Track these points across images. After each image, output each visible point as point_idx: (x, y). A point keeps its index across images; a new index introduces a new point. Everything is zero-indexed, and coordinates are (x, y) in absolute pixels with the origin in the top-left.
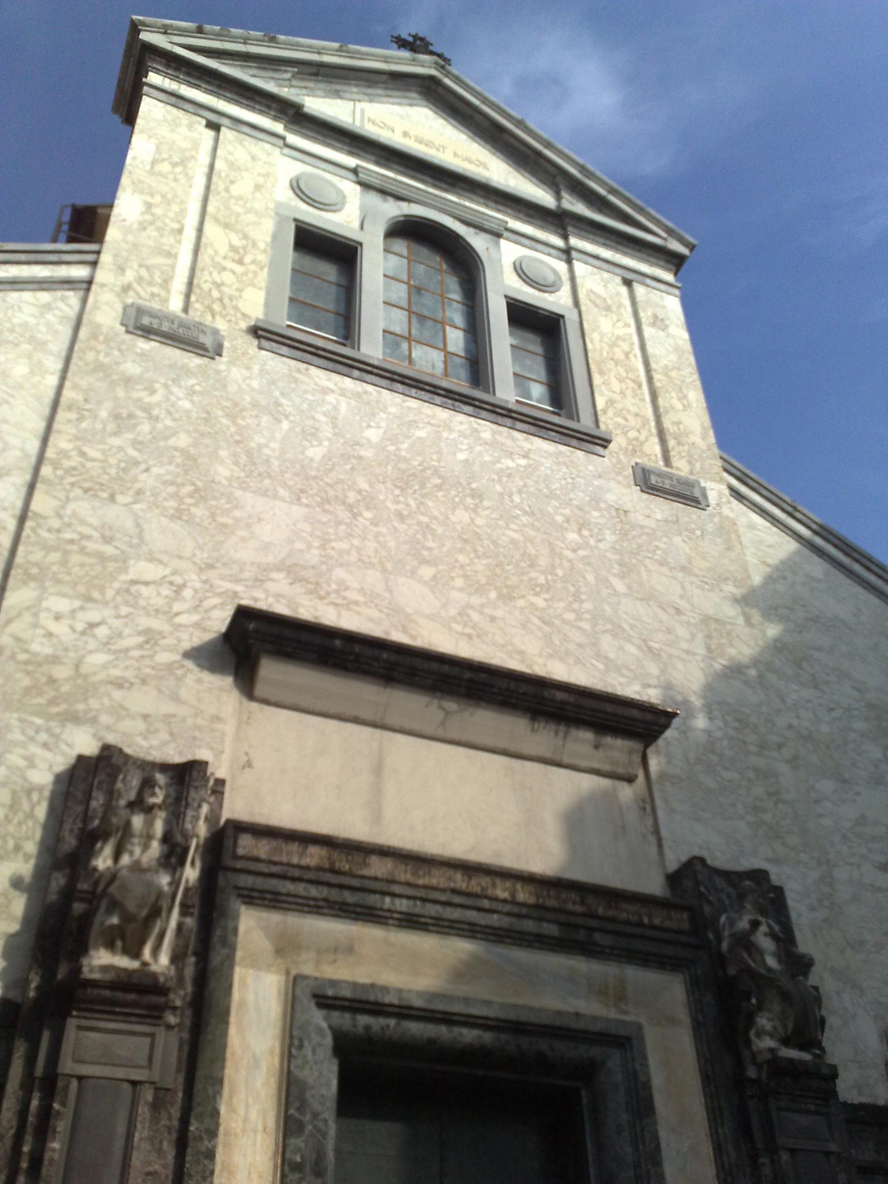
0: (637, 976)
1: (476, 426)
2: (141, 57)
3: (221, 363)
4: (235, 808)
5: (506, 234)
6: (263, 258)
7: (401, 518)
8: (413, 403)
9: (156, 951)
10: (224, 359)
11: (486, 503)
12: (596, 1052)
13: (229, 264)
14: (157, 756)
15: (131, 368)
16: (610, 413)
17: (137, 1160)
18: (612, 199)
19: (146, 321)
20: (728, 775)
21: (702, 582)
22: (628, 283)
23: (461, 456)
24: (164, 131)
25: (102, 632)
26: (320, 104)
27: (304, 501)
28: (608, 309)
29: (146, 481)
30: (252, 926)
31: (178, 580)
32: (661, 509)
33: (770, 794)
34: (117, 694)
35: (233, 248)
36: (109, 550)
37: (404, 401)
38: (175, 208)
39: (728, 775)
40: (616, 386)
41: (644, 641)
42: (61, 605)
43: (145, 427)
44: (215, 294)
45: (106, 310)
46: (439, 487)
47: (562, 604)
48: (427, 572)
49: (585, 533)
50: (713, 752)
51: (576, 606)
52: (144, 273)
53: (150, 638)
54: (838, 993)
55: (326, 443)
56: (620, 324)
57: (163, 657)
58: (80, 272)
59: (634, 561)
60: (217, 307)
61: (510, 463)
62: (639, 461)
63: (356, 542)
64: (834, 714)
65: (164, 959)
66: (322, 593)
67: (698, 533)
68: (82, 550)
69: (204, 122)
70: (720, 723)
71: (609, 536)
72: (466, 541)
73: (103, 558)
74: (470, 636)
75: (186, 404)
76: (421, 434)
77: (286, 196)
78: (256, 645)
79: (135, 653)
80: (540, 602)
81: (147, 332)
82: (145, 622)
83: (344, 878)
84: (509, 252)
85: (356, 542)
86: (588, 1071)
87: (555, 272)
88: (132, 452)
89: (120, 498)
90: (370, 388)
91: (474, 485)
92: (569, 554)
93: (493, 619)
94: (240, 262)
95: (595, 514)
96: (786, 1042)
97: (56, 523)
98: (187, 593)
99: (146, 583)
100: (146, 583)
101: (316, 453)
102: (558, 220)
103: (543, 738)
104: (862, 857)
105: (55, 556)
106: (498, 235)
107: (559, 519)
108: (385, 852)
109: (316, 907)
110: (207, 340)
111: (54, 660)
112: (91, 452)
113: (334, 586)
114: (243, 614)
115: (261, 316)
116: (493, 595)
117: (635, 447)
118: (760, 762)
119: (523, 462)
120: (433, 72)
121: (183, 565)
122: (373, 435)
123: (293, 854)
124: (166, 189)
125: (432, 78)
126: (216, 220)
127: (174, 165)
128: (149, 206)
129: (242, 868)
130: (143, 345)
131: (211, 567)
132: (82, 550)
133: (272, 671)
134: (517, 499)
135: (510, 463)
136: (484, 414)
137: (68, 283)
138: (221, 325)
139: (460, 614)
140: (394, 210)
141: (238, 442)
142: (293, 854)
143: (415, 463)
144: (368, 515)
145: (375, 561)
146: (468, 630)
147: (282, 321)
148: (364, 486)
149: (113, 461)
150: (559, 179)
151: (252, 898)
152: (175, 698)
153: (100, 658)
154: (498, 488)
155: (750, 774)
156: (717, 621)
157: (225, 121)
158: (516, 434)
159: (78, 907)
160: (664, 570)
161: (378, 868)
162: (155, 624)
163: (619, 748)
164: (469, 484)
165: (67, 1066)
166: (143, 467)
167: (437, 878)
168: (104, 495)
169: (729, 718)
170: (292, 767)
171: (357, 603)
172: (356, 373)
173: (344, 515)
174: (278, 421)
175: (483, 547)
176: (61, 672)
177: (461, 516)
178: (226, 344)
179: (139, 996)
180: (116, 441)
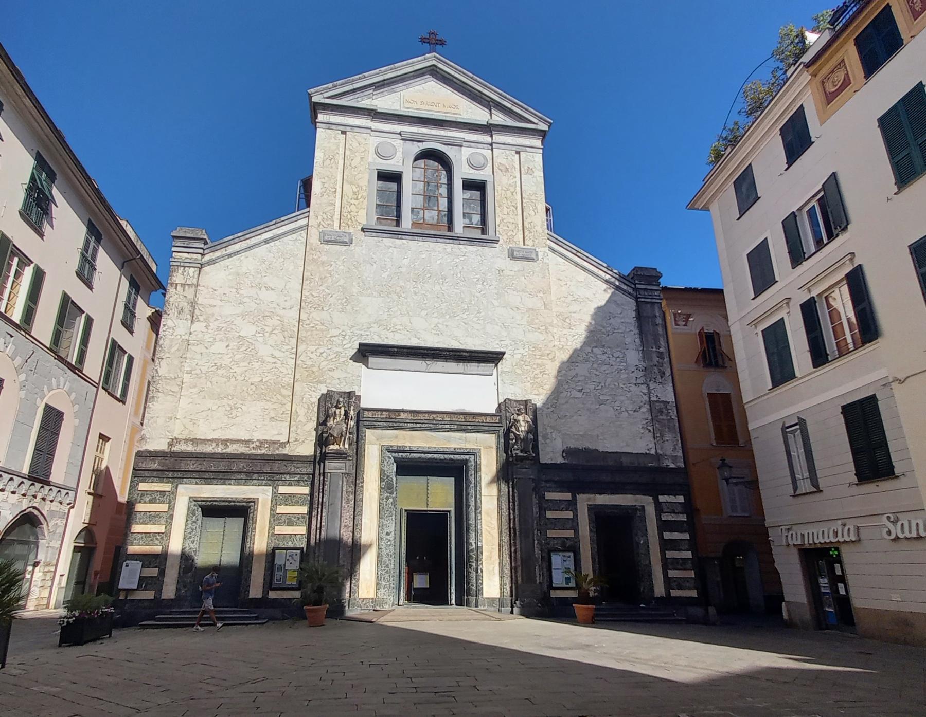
2: (316, 108)
3: (352, 247)
4: (364, 404)
5: (464, 144)
7: (415, 293)
8: (421, 243)
9: (344, 445)
12: (467, 457)
13: (353, 201)
14: (343, 390)
15: (324, 258)
17: (344, 489)
18: (514, 108)
19: (326, 237)
22: (518, 153)
23: (439, 262)
24: (326, 141)
25: (324, 355)
26: (384, 102)
29: (332, 300)
30: (370, 435)
32: (518, 265)
34: (330, 373)
35: (354, 193)
36: (324, 328)
38: (333, 181)
40: (505, 211)
42: (313, 348)
43: (330, 280)
45: (314, 239)
48: (424, 313)
52: (324, 216)
53: (338, 354)
57: (342, 360)
58: (304, 222)
60: (350, 223)
65: (347, 446)
68: (316, 330)
71: (495, 283)
73: (322, 331)
75: (342, 267)
76: (424, 256)
77: (372, 157)
78: (366, 352)
80: (464, 316)
81: (327, 242)
82: (336, 349)
83: (392, 419)
84: (466, 152)
86: (466, 462)
87: (485, 157)
90: (405, 241)
92: (478, 294)
94: (357, 199)
96: (521, 452)
97: (308, 322)
98: (347, 337)
101: (385, 275)
102: (487, 129)
103: (461, 366)
105: (309, 333)
108: (404, 411)
109: (386, 428)
110: (346, 240)
111: (313, 366)
112: (315, 294)
114: (360, 345)
115: (365, 223)
117: (510, 239)
118: (539, 361)
119: (463, 258)
120: (434, 62)
121: (345, 328)
123: (378, 415)
124: (329, 173)
125: (434, 65)
126: (347, 181)
128: (323, 183)
129: (364, 420)
130: (327, 247)
131: (353, 327)
132: (316, 330)
133: (372, 360)
137: (301, 228)
138: (351, 230)
140: (417, 148)
142: (378, 415)
147: (373, 223)
148: (402, 284)
151: (369, 427)
152: (346, 372)
153: (325, 363)
155: (535, 366)
157: (348, 129)
158: (461, 246)
159: (325, 435)
160: (515, 293)
161: (403, 416)
162: (340, 349)
165: (327, 471)
167: (421, 417)
170: (382, 388)
173: (396, 297)
176: (315, 369)
177: (438, 287)
179: (340, 455)
180: (321, 288)
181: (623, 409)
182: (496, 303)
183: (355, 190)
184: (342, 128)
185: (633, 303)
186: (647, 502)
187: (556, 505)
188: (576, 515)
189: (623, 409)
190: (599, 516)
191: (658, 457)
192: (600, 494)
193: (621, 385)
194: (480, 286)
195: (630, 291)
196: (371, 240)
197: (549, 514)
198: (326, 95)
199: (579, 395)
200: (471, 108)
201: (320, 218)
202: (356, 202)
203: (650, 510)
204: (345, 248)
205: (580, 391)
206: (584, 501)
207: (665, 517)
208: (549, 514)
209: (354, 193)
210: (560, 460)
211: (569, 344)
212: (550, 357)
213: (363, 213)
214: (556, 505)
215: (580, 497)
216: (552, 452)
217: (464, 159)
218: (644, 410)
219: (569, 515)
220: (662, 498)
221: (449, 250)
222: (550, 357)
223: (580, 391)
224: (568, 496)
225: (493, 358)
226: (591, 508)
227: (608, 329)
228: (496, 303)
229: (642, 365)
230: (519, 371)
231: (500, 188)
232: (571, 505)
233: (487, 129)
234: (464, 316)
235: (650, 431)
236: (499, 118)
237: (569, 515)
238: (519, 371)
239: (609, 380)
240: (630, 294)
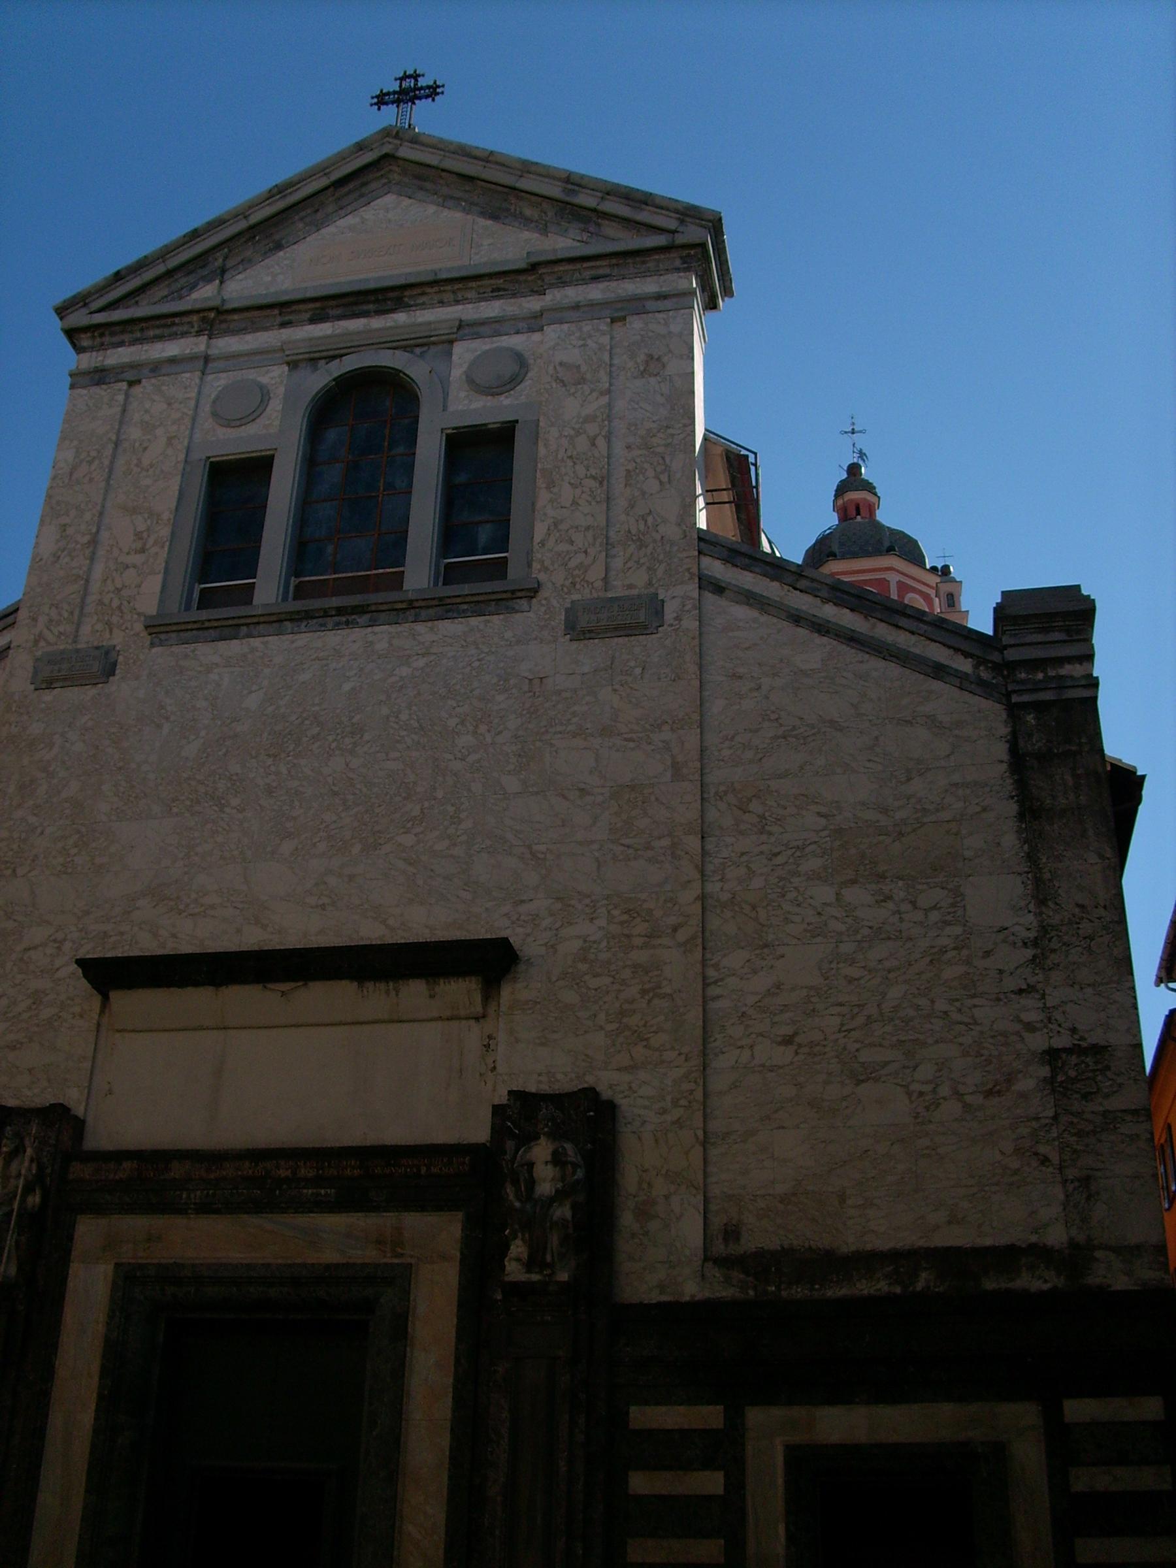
0: (414, 1222)
1: (371, 638)
6: (165, 532)
8: (302, 639)
10: (117, 677)
11: (367, 737)
16: (550, 543)
20: (594, 983)
21: (626, 740)
23: (347, 687)
27: (175, 810)
28: (582, 380)
31: (60, 936)
32: (593, 654)
33: (644, 992)
37: (293, 642)
39: (594, 983)
41: (529, 847)
44: (116, 603)
46: (315, 738)
47: (437, 833)
48: (287, 847)
49: (483, 728)
50: (584, 960)
51: (451, 831)
52: (54, 613)
54: (667, 1197)
55: (203, 733)
56: (595, 394)
59: (538, 744)
60: (115, 619)
61: (405, 671)
62: (576, 597)
63: (220, 839)
64: (779, 860)
66: (182, 907)
67: (638, 671)
69: (124, 385)
70: (602, 922)
72: (336, 794)
74: (323, 907)
78: (109, 975)
79: (25, 1016)
80: (408, 840)
81: (49, 684)
83: (157, 1179)
84: (464, 352)
85: (220, 839)
88: (32, 820)
89: (20, 872)
91: (354, 721)
93: (351, 878)
94: (143, 550)
95: (500, 698)
99: (35, 948)
100: (35, 948)
104: (761, 1035)
106: (451, 342)
107: (452, 722)
113: (194, 896)
116: (356, 849)
118: (641, 956)
119: (421, 662)
122: (252, 702)
127: (90, 463)
128: (64, 527)
130: (48, 696)
131: (87, 913)
134: (404, 717)
135: (405, 671)
136: (383, 616)
138: (118, 639)
139: (317, 884)
141: (120, 768)
143: (293, 718)
144: (235, 802)
145: (236, 853)
146: (326, 900)
149: (16, 835)
150: (545, 205)
154: (385, 711)
156: (633, 788)
158: (420, 628)
161: (177, 1170)
163: (461, 991)
164: (351, 718)
166: (39, 830)
168: (9, 872)
169: (616, 912)
171: (212, 907)
172: (244, 629)
174: (159, 726)
175: (354, 794)
178: (121, 659)
181: (945, 1090)
182: (512, 784)
183: (141, 527)
184: (130, 375)
185: (993, 712)
186: (1018, 1426)
187: (671, 1450)
188: (736, 1485)
189: (945, 1090)
190: (818, 1475)
191: (1074, 1259)
192: (832, 1401)
193: (941, 1005)
194: (466, 740)
195: (985, 674)
196: (162, 657)
197: (640, 1483)
198: (95, 306)
199: (783, 1055)
200: (488, 621)
201: (42, 620)
202: (138, 559)
203: (1029, 1455)
204: (91, 692)
205: (788, 1041)
206: (772, 1433)
207: (1082, 1480)
208: (640, 1483)
209: (138, 535)
210: (691, 1290)
211: (757, 883)
212: (681, 936)
213: (154, 584)
214: (671, 1450)
215: (755, 1416)
216: (665, 1257)
217: (457, 373)
218: (1026, 1084)
219: (712, 1482)
220: (1077, 1410)
221: (381, 646)
222: (681, 936)
223: (788, 1041)
224: (710, 1416)
225: (488, 962)
226: (801, 1460)
227: (900, 815)
228: (512, 784)
229: (1025, 924)
230: (570, 996)
231: (554, 432)
232: (723, 1449)
233: (532, 274)
234: (408, 840)
235: (1045, 1161)
236: (563, 242)
237: (712, 1482)
238: (570, 996)
239: (895, 993)
240: (981, 683)
